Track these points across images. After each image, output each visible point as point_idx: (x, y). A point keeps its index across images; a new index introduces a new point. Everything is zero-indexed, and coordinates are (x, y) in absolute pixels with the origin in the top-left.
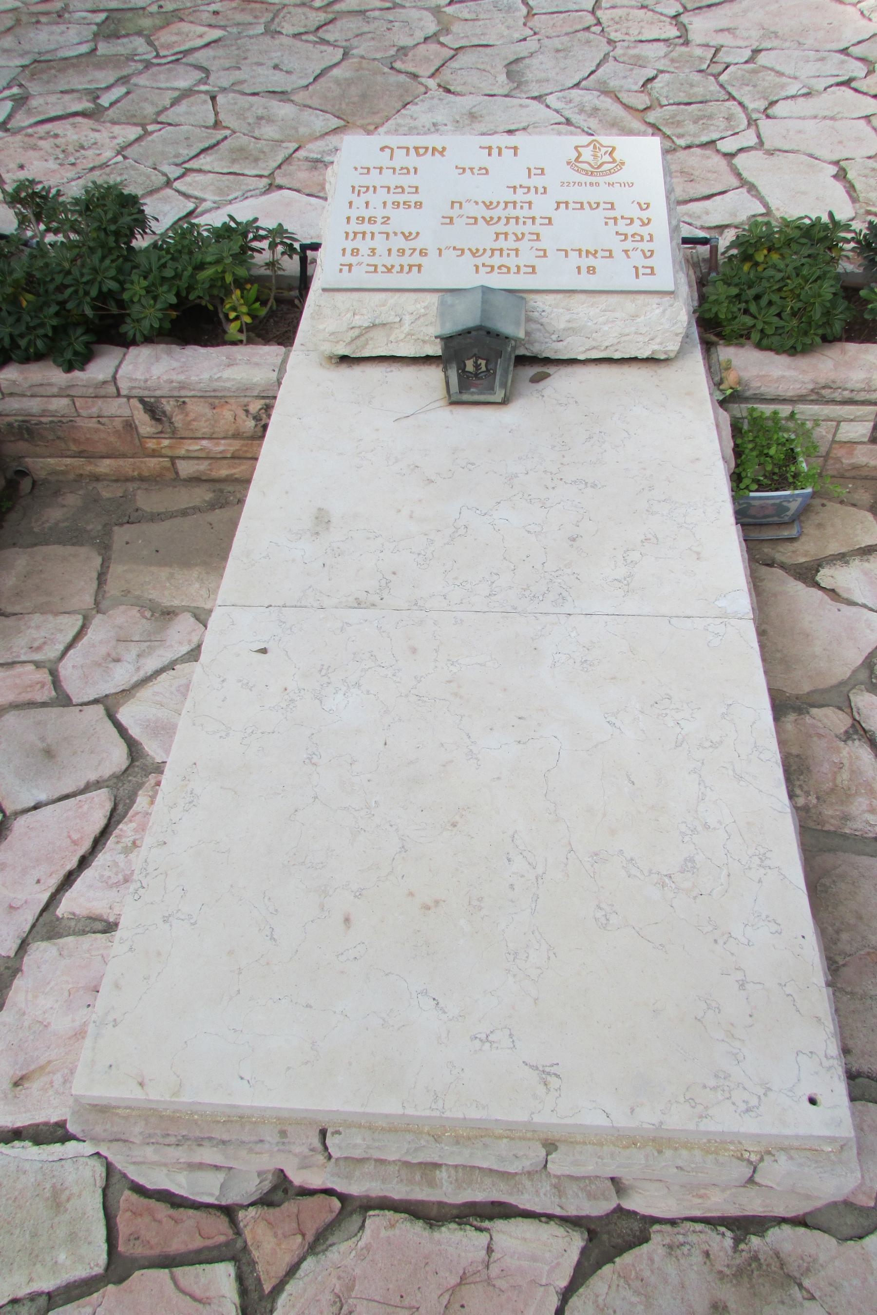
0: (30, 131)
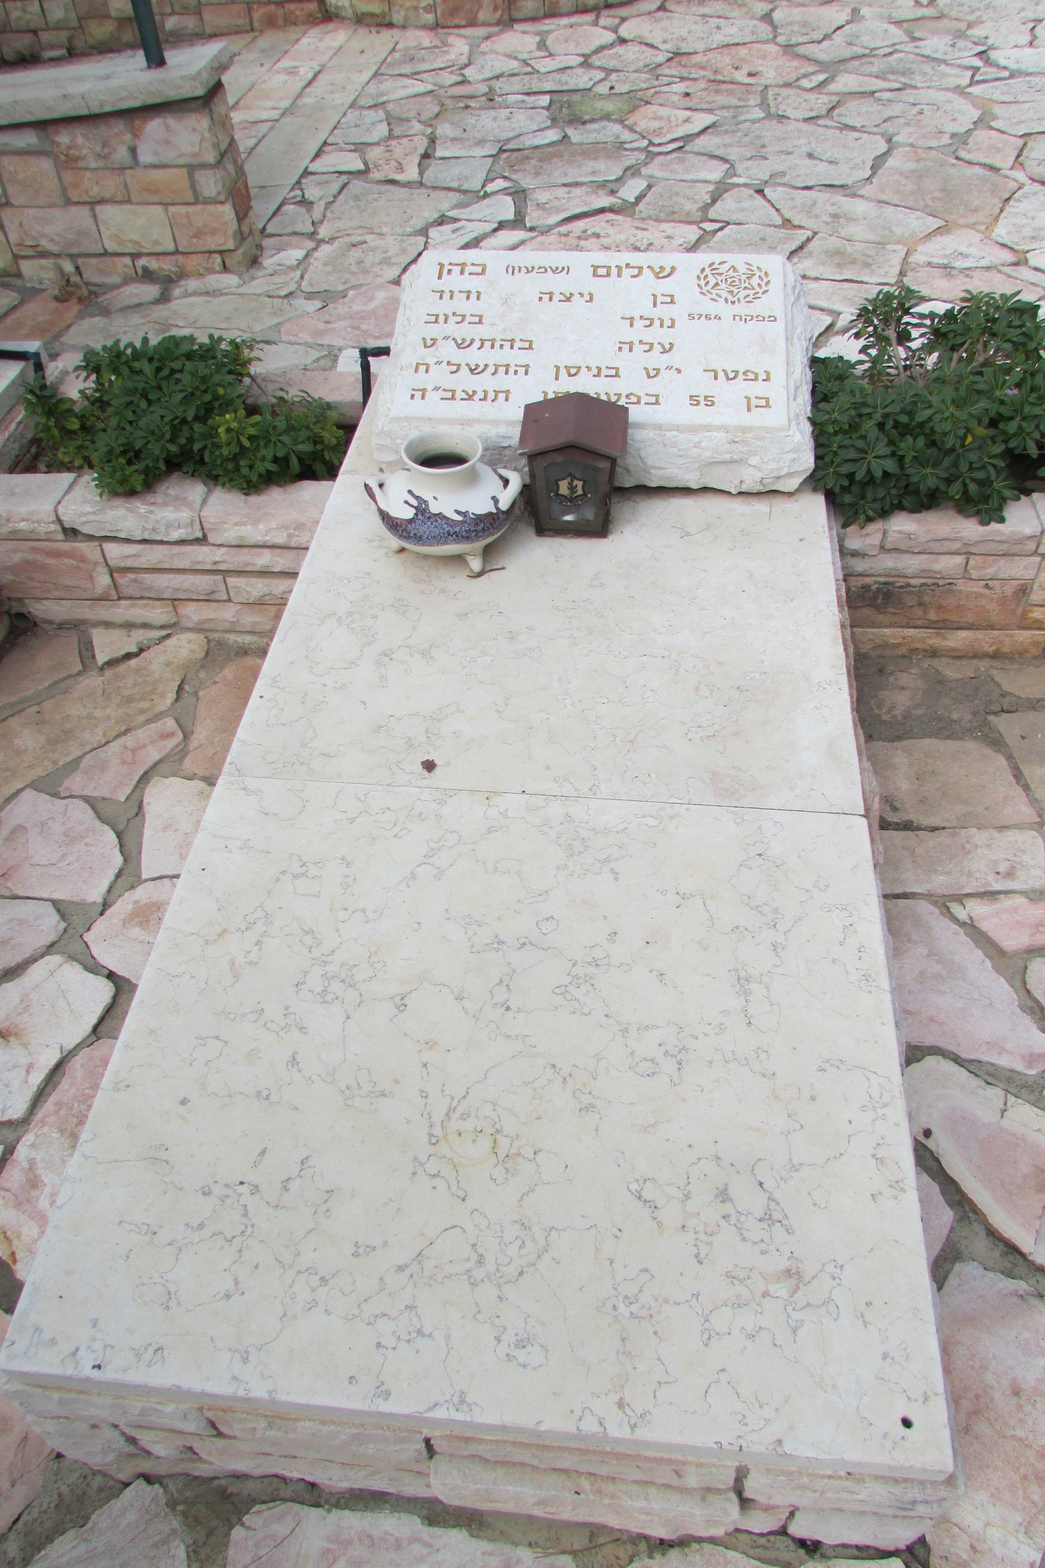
0: (563, 229)
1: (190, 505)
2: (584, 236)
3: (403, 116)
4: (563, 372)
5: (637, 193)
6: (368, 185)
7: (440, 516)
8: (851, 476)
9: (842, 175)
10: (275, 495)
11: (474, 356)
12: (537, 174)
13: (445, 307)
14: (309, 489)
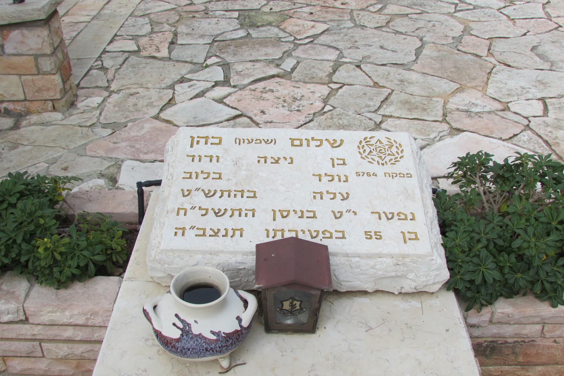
0: (252, 87)
1: (17, 299)
2: (264, 91)
3: (159, 21)
4: (278, 215)
5: (291, 66)
6: (139, 59)
7: (200, 336)
8: (472, 282)
9: (400, 58)
10: (78, 288)
11: (217, 203)
12: (235, 54)
13: (196, 167)
14: (103, 284)
